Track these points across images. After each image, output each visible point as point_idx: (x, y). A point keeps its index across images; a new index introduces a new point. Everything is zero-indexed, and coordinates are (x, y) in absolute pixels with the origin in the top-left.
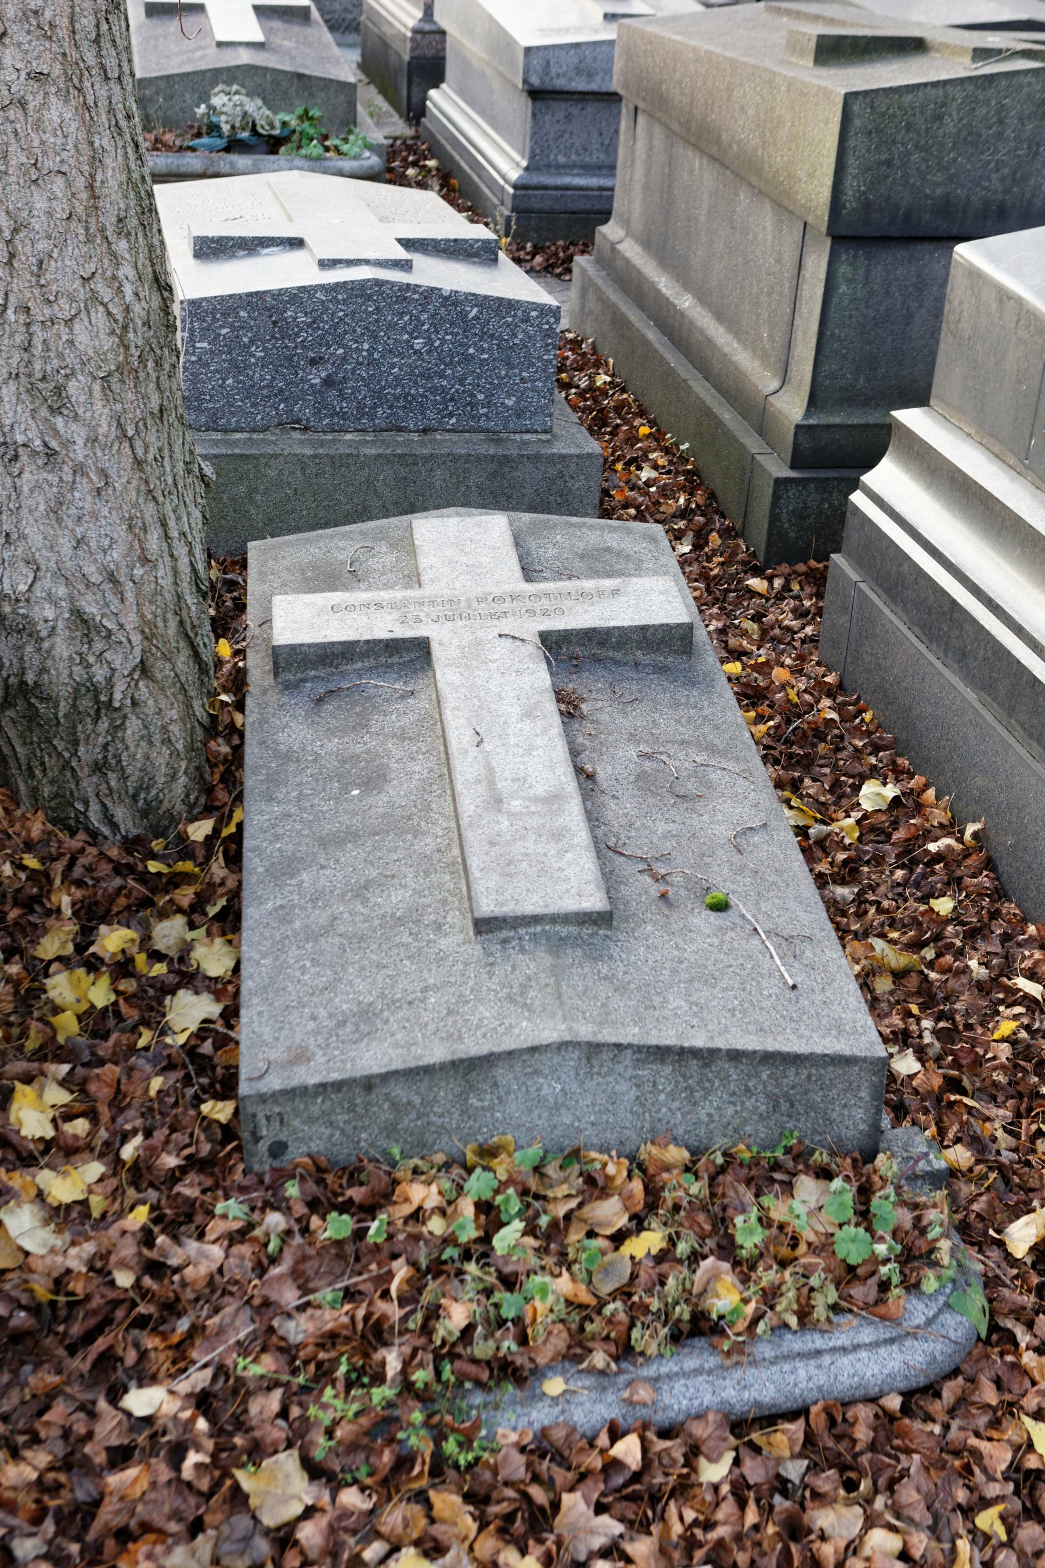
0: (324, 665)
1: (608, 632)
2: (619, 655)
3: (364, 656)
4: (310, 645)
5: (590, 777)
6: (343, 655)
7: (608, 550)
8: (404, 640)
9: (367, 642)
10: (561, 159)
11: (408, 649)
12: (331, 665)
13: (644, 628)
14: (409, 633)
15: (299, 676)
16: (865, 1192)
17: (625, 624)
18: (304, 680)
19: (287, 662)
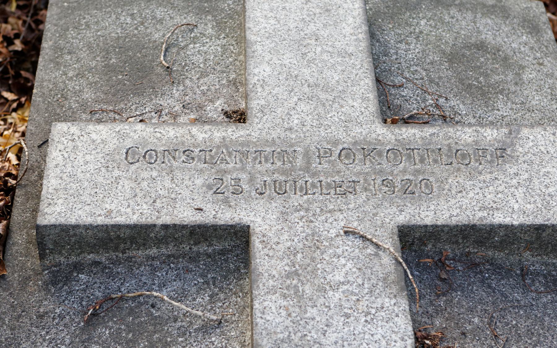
0: (107, 250)
1: (492, 229)
2: (499, 255)
3: (160, 242)
4: (87, 227)
5: (411, 117)
6: (133, 240)
7: (481, 46)
8: (215, 228)
9: (165, 227)
10: (176, 31)
11: (220, 238)
12: (116, 249)
13: (539, 229)
14: (227, 217)
15: (73, 259)
16: (497, 209)
17: (516, 220)
18: (78, 267)
19: (55, 243)
